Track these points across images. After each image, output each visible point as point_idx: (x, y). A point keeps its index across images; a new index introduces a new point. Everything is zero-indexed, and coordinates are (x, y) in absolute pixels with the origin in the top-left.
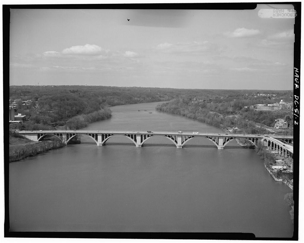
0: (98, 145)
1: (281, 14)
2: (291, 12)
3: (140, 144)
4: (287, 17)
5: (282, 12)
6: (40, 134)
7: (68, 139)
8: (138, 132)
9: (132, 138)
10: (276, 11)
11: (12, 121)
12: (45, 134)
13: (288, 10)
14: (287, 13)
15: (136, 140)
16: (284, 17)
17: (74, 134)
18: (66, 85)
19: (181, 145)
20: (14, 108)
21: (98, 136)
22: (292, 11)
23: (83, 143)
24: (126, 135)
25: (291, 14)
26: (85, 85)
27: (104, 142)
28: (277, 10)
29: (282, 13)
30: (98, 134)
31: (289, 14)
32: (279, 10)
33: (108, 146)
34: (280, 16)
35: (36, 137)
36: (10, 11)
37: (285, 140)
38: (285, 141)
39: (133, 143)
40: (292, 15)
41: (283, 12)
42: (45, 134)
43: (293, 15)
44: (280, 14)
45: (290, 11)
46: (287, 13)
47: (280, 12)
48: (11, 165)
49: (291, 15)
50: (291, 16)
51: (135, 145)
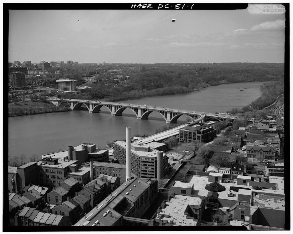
0: (167, 122)
1: (270, 10)
2: (280, 8)
3: (114, 114)
4: (277, 13)
5: (271, 8)
6: (175, 113)
7: (142, 114)
8: (166, 110)
9: (163, 114)
10: (266, 7)
11: (72, 91)
12: (78, 102)
13: (277, 6)
14: (276, 9)
15: (166, 117)
16: (273, 13)
17: (149, 110)
18: (268, 63)
19: (140, 117)
20: (74, 81)
21: (138, 110)
22: (281, 7)
23: (123, 116)
24: (158, 111)
25: (280, 10)
26: (247, 62)
27: (93, 109)
28: (266, 6)
29: (271, 9)
30: (90, 104)
31: (279, 10)
32: (269, 6)
33: (149, 120)
34: (269, 11)
35: (58, 103)
36: (9, 12)
37: (220, 119)
38: (221, 120)
39: (162, 118)
40: (281, 11)
41: (272, 8)
42: (179, 114)
43: (282, 11)
44: (269, 10)
45: (279, 7)
46: (276, 9)
47: (269, 8)
48: (10, 119)
49: (280, 11)
50: (280, 12)
51: (166, 121)
